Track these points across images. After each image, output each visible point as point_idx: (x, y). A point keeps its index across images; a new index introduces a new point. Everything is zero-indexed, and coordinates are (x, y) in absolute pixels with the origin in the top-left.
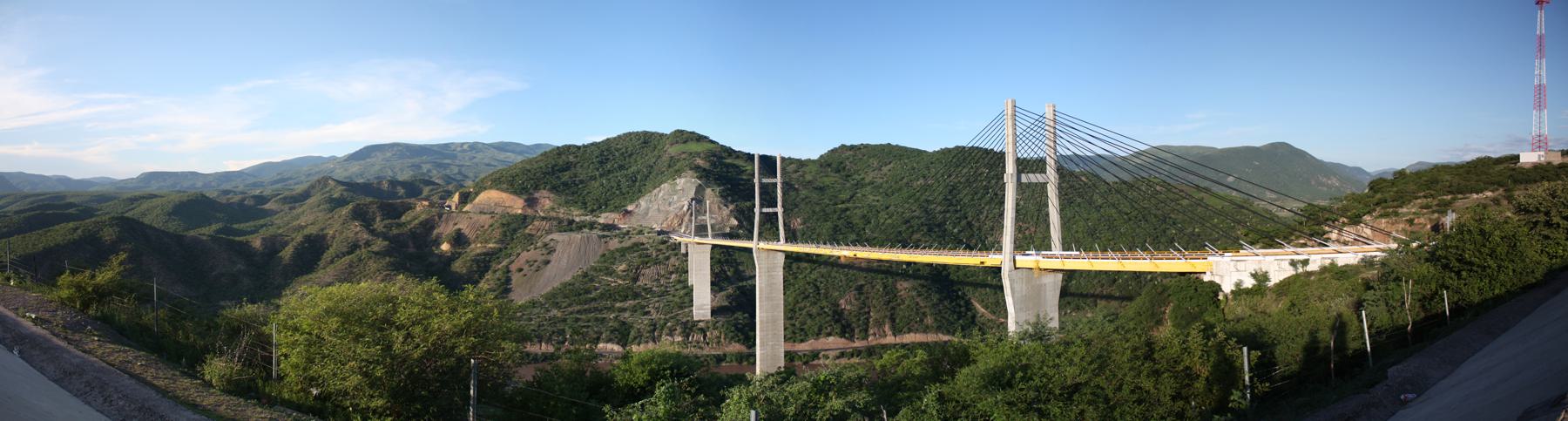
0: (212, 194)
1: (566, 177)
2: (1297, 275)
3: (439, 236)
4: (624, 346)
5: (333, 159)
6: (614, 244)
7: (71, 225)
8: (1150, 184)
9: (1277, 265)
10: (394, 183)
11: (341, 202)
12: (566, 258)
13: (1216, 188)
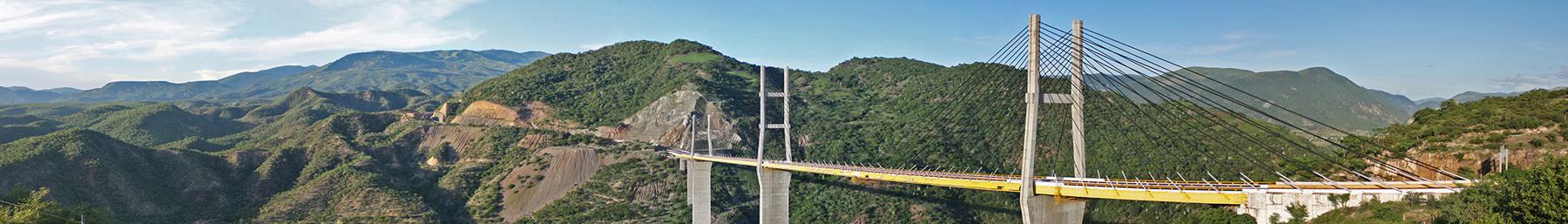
0: (184, 105)
1: (561, 87)
2: (1337, 211)
3: (425, 150)
6: (610, 159)
7: (31, 139)
8: (1180, 108)
12: (563, 174)
13: (1250, 114)
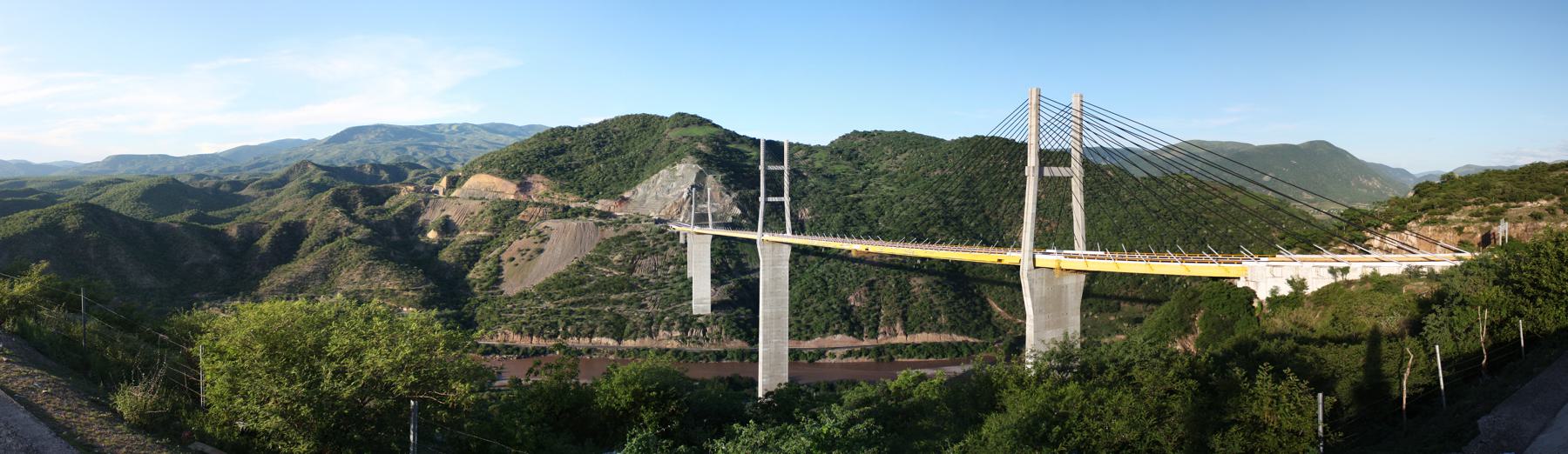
0: (184, 178)
1: (560, 160)
2: (1337, 284)
3: (425, 223)
4: (619, 340)
5: (313, 142)
6: (610, 233)
7: (31, 212)
8: (1180, 180)
9: (1315, 272)
10: (377, 167)
11: (319, 188)
12: (556, 247)
13: (1250, 187)
